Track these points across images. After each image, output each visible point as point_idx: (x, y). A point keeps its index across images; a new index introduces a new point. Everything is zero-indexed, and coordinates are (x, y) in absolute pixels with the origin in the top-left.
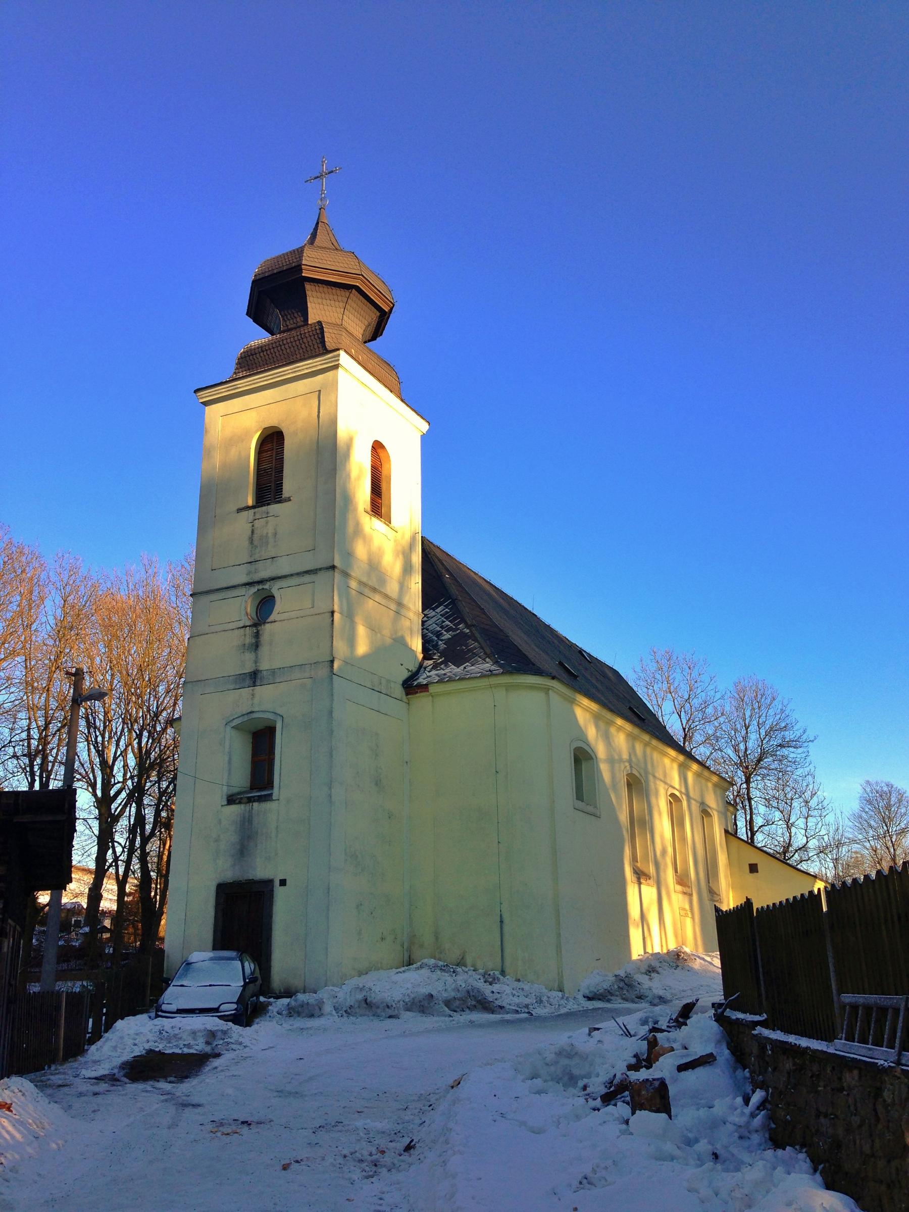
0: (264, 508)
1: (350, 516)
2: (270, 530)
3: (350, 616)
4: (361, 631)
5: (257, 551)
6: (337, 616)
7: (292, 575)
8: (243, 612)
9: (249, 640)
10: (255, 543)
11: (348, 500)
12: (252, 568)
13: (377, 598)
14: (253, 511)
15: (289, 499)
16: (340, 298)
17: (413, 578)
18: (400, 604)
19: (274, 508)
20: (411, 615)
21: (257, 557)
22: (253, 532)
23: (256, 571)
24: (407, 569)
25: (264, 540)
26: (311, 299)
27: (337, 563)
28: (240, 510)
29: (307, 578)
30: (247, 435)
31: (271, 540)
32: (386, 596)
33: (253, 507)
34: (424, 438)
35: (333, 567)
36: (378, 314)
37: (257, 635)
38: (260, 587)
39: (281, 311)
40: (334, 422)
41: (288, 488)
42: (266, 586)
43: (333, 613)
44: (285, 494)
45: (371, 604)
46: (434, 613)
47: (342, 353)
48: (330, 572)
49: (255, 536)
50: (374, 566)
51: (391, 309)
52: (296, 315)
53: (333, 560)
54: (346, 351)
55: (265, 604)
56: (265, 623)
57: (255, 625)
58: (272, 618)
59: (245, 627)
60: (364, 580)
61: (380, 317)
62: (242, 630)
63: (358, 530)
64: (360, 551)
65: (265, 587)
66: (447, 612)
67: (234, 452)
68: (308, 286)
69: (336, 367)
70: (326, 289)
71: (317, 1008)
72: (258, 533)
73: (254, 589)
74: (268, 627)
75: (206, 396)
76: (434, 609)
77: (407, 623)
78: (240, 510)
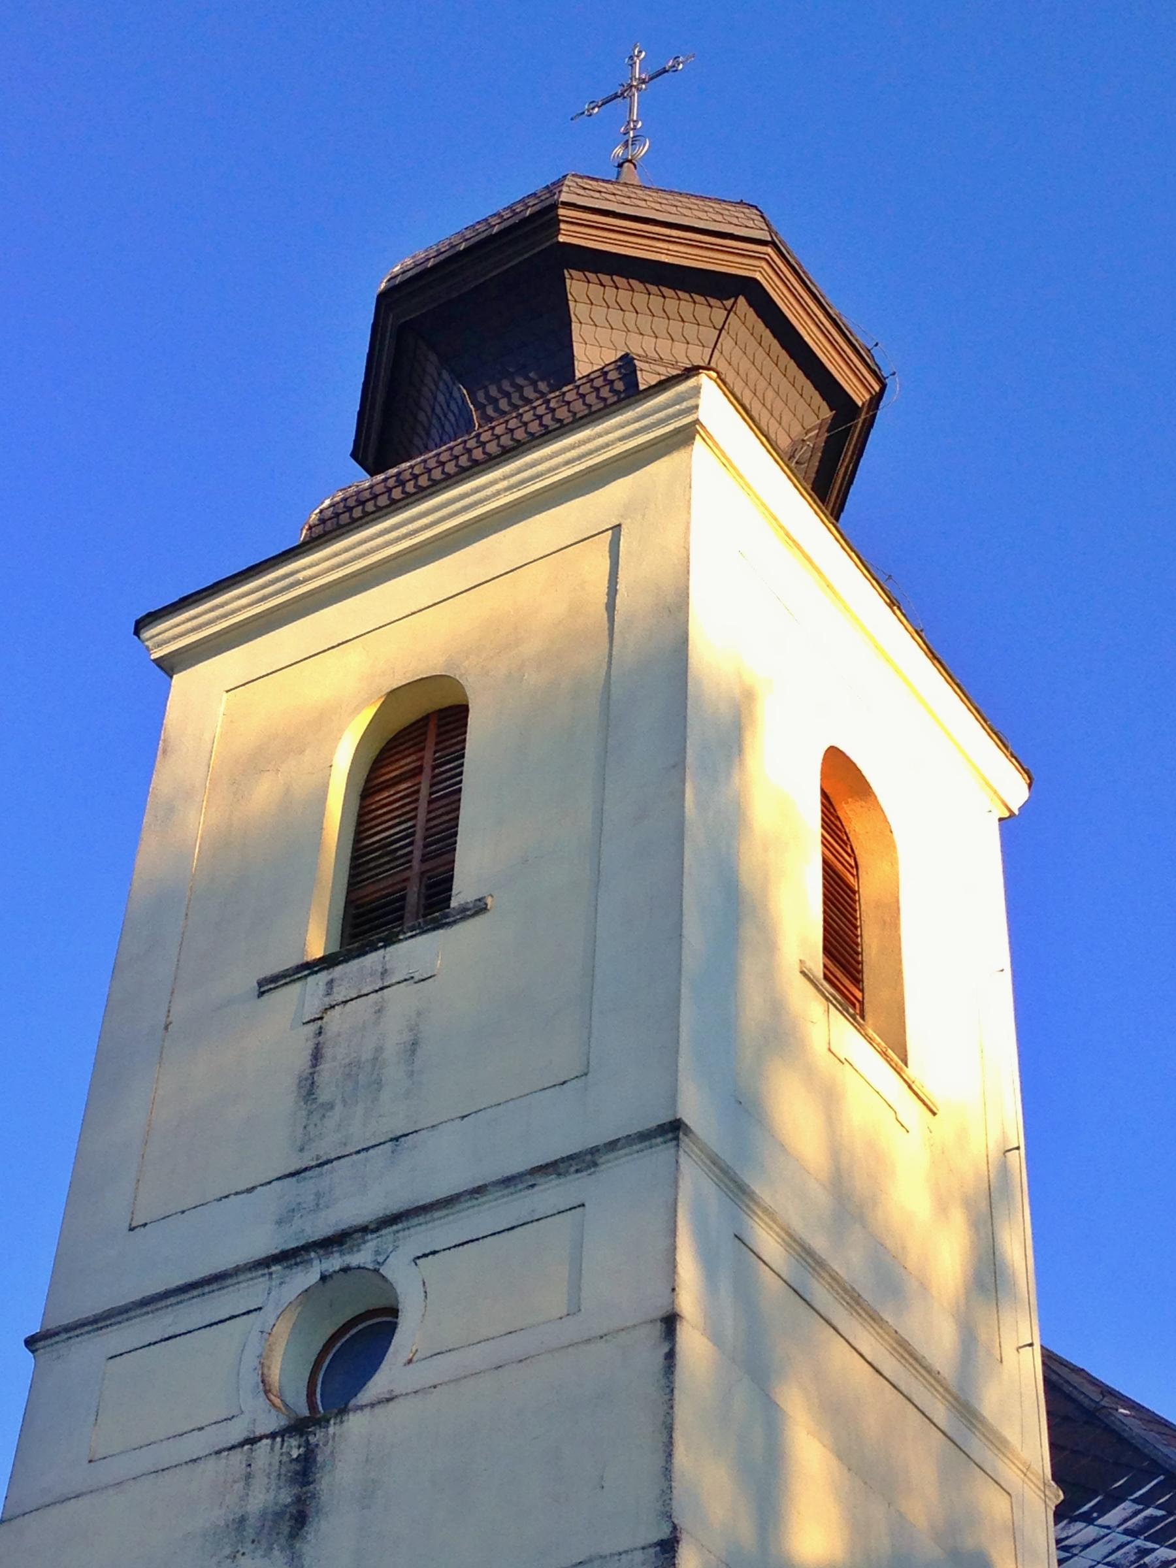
0: (372, 960)
1: (750, 968)
2: (394, 1034)
3: (754, 1365)
4: (810, 1457)
5: (332, 1121)
6: (692, 1341)
7: (478, 1191)
8: (251, 1379)
9: (266, 1494)
10: (324, 1095)
11: (739, 908)
12: (307, 1188)
13: (868, 1342)
14: (323, 977)
15: (479, 908)
16: (690, 330)
17: (1007, 1318)
18: (966, 1411)
19: (414, 952)
20: (1010, 1474)
21: (325, 1147)
22: (317, 1056)
23: (320, 1203)
24: (988, 1276)
25: (365, 1078)
26: (588, 330)
27: (693, 1108)
28: (268, 985)
29: (551, 1194)
30: (322, 723)
31: (394, 1072)
32: (905, 1350)
33: (327, 962)
34: (1013, 829)
35: (674, 1129)
36: (827, 413)
37: (304, 1471)
38: (334, 1262)
39: (473, 355)
40: (675, 610)
41: (471, 871)
42: (362, 1257)
43: (670, 1322)
44: (463, 892)
45: (846, 1359)
46: (1091, 1532)
47: (706, 382)
48: (661, 1153)
49: (325, 1067)
50: (850, 1200)
51: (876, 400)
52: (529, 392)
53: (673, 1097)
54: (722, 381)
55: (356, 1344)
56: (343, 1411)
57: (298, 1427)
58: (377, 1385)
59: (252, 1441)
60: (819, 1243)
61: (834, 423)
62: (238, 1457)
63: (781, 1036)
64: (795, 1116)
65: (354, 1260)
66: (1154, 1520)
67: (264, 792)
68: (577, 286)
69: (685, 436)
70: (640, 296)
71: (250, 1532)
72: (336, 1055)
73: (307, 1277)
74: (355, 1424)
75: (170, 636)
76: (1088, 1519)
77: (996, 1505)
78: (268, 985)
